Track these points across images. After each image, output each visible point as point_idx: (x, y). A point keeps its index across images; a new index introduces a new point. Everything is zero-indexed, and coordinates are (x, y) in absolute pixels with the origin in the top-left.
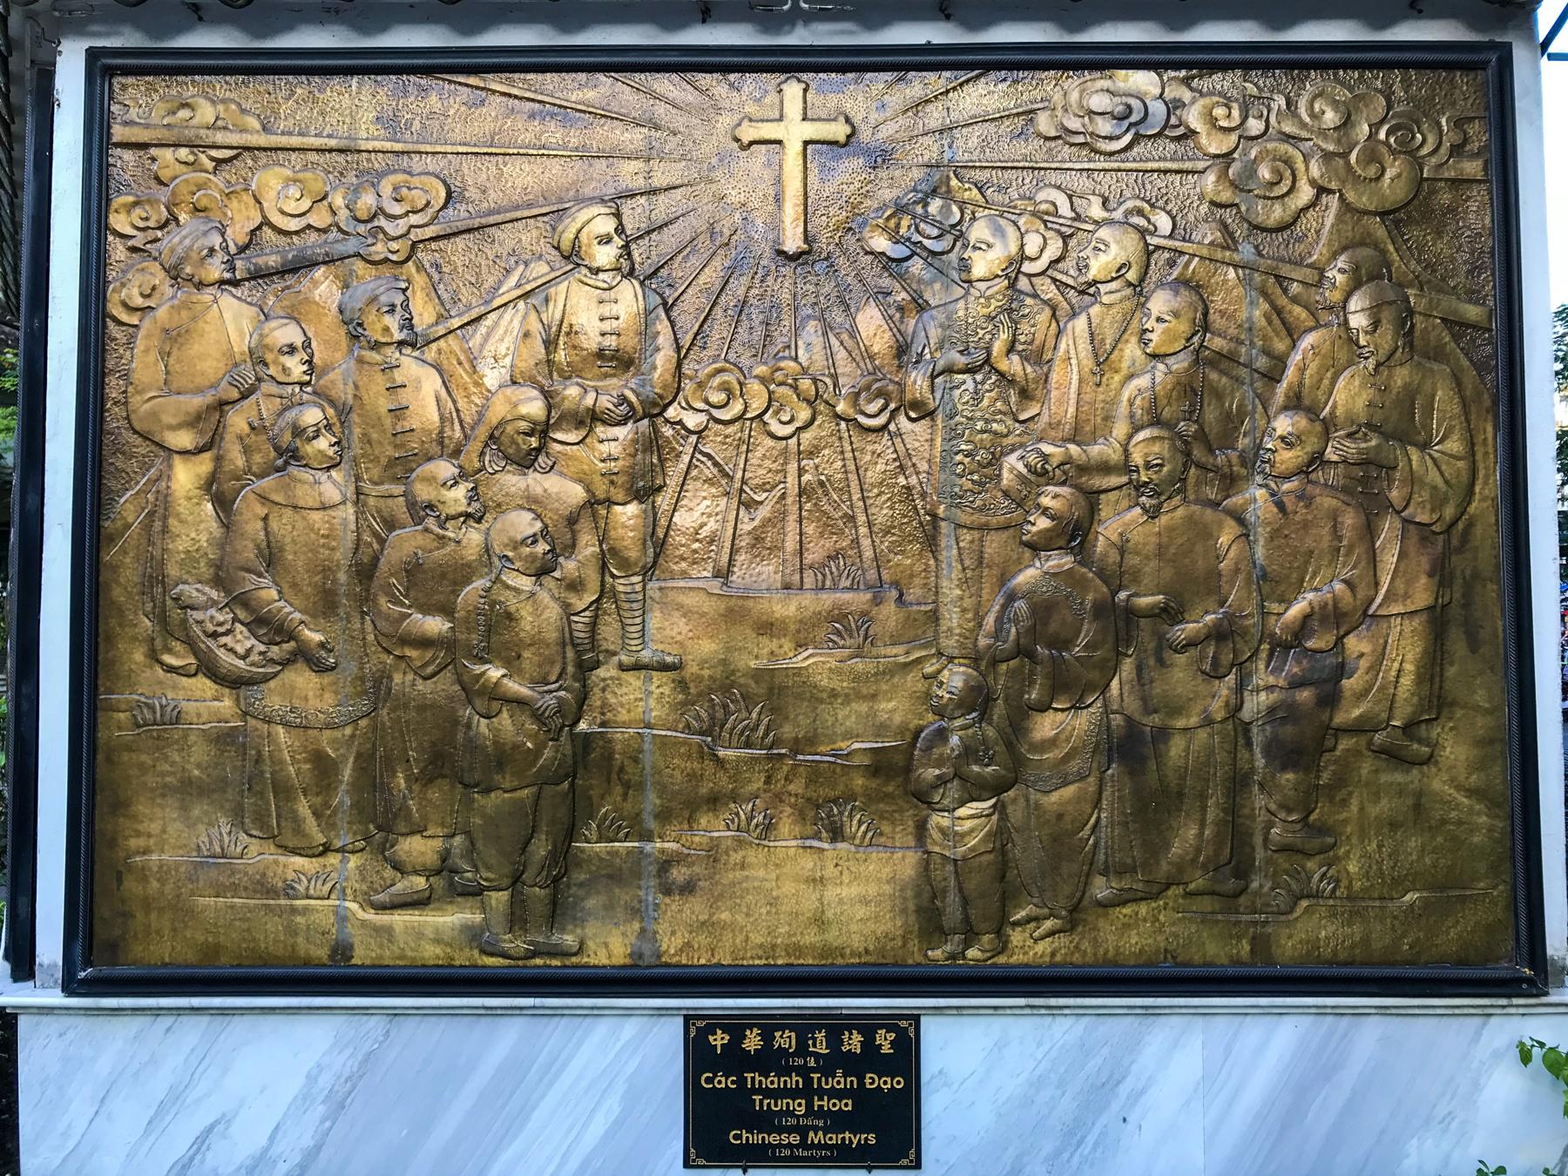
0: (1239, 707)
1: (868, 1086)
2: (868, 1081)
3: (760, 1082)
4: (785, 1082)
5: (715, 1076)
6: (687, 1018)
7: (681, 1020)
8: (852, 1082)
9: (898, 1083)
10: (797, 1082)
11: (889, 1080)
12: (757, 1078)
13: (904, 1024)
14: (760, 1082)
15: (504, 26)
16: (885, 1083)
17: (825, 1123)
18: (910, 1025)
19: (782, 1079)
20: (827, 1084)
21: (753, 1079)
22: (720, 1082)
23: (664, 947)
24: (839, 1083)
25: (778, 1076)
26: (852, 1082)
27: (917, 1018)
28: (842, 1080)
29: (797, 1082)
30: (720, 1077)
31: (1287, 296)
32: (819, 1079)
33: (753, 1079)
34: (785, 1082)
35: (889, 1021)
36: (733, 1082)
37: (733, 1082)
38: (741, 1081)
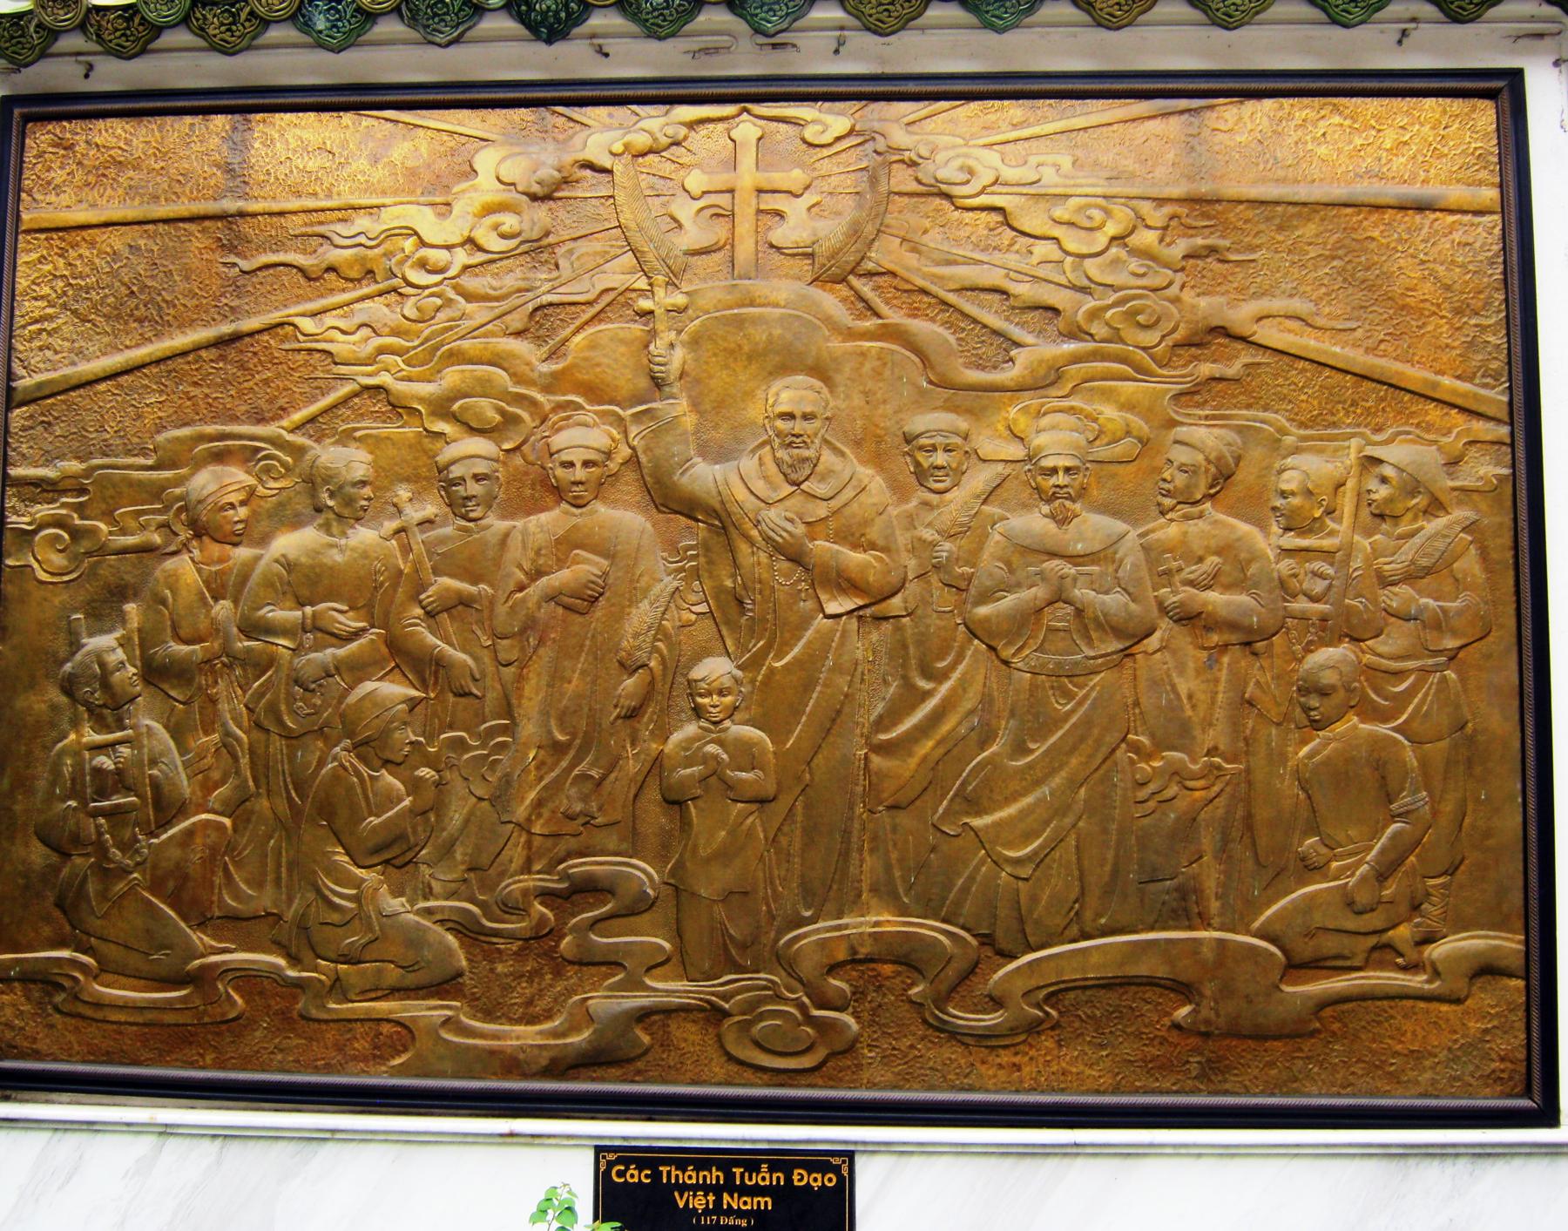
0: (455, 485)
1: (796, 1183)
2: (796, 1177)
3: (677, 1176)
4: (705, 1177)
5: (627, 1169)
6: (599, 1150)
7: (591, 1154)
8: (778, 1178)
9: (830, 1180)
10: (718, 1177)
11: (819, 1176)
12: (674, 1173)
13: (835, 1161)
14: (677, 1176)
15: (65, 1097)
16: (815, 1180)
17: (749, 1222)
18: (844, 1162)
19: (701, 1174)
20: (750, 1179)
21: (669, 1173)
22: (632, 1176)
23: (758, 338)
24: (764, 1179)
25: (697, 1170)
26: (778, 1178)
27: (850, 1155)
28: (767, 1176)
29: (718, 1177)
30: (633, 1170)
31: (528, 586)
32: (742, 1175)
33: (669, 1173)
34: (705, 1177)
35: (817, 1160)
36: (647, 1176)
37: (647, 1176)
38: (656, 1175)
